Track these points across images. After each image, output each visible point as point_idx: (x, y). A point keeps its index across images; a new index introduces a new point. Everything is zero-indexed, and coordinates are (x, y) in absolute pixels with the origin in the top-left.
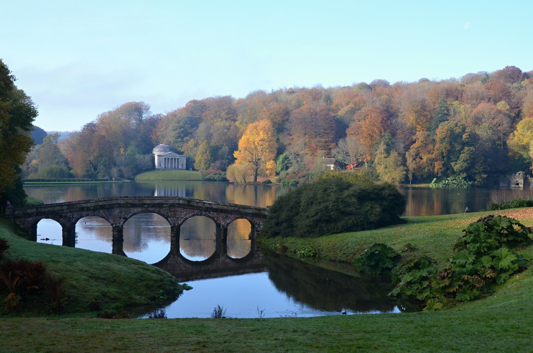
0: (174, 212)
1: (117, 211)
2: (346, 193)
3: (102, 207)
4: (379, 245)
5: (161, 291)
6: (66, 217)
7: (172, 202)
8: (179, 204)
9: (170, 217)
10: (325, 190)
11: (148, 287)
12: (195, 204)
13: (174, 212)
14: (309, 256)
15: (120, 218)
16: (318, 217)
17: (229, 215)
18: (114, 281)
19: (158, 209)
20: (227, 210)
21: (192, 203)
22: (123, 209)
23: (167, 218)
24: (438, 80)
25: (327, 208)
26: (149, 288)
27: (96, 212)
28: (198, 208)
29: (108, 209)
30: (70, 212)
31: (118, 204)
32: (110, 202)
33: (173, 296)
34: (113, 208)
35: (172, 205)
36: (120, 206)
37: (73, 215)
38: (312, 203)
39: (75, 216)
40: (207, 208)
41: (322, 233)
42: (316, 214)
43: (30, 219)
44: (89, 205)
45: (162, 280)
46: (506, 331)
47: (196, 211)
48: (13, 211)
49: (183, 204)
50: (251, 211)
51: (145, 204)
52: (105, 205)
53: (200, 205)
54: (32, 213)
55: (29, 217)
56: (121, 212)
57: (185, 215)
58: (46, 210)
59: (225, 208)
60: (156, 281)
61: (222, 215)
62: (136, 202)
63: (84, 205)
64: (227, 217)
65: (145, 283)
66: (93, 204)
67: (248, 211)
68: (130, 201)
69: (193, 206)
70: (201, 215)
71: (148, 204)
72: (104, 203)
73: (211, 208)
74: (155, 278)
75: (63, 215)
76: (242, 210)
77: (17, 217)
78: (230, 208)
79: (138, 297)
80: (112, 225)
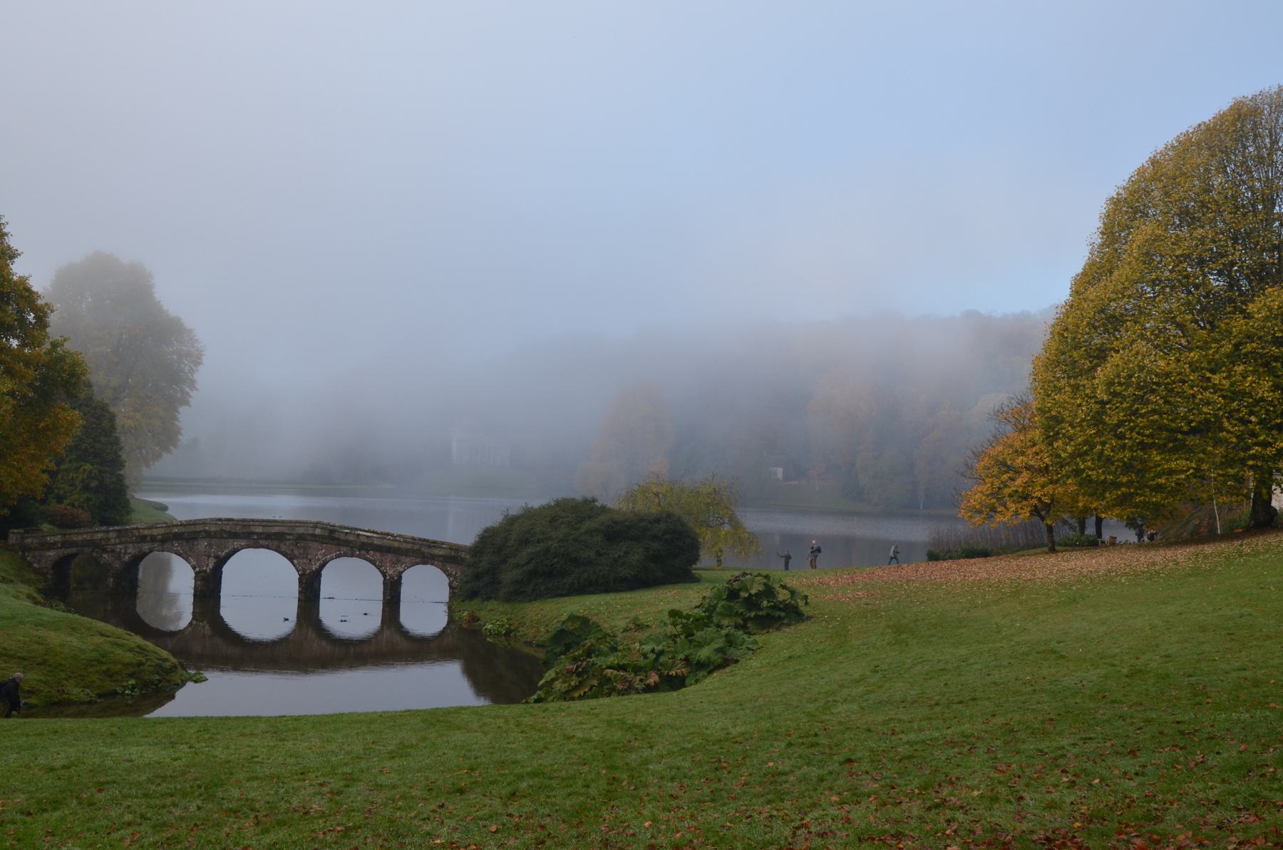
0: (304, 548)
1: (203, 545)
2: (588, 525)
3: (178, 537)
4: (578, 618)
5: (132, 682)
6: (113, 551)
7: (301, 530)
8: (313, 535)
9: (297, 558)
10: (553, 520)
11: (109, 674)
12: (342, 537)
13: (304, 548)
14: (499, 634)
15: (209, 556)
16: (530, 567)
17: (403, 558)
18: (44, 663)
19: (275, 543)
20: (399, 549)
21: (336, 535)
22: (213, 541)
23: (291, 560)
24: (165, 308)
25: (548, 550)
26: (111, 676)
27: (167, 545)
28: (346, 543)
29: (187, 540)
30: (121, 543)
31: (205, 531)
32: (192, 529)
33: (164, 693)
34: (196, 539)
35: (301, 537)
36: (209, 535)
37: (126, 548)
38: (527, 542)
39: (129, 550)
40: (363, 544)
41: (537, 596)
42: (528, 563)
43: (51, 553)
44: (155, 532)
45: (140, 664)
46: (1217, 803)
47: (343, 549)
48: (23, 538)
49: (321, 537)
50: (442, 552)
51: (254, 533)
52: (183, 533)
53: (351, 538)
54: (55, 543)
55: (49, 549)
56: (210, 545)
57: (325, 555)
58: (80, 538)
59: (396, 544)
60: (127, 665)
61: (390, 557)
62: (238, 529)
63: (146, 532)
64: (398, 561)
65: (104, 668)
66: (162, 531)
67: (436, 552)
68: (228, 528)
69: (338, 539)
70: (352, 556)
71: (258, 534)
72: (182, 530)
73: (371, 544)
74: (127, 660)
75: (109, 548)
76: (425, 550)
77: (30, 549)
78: (404, 546)
79: (76, 691)
80: (194, 568)
